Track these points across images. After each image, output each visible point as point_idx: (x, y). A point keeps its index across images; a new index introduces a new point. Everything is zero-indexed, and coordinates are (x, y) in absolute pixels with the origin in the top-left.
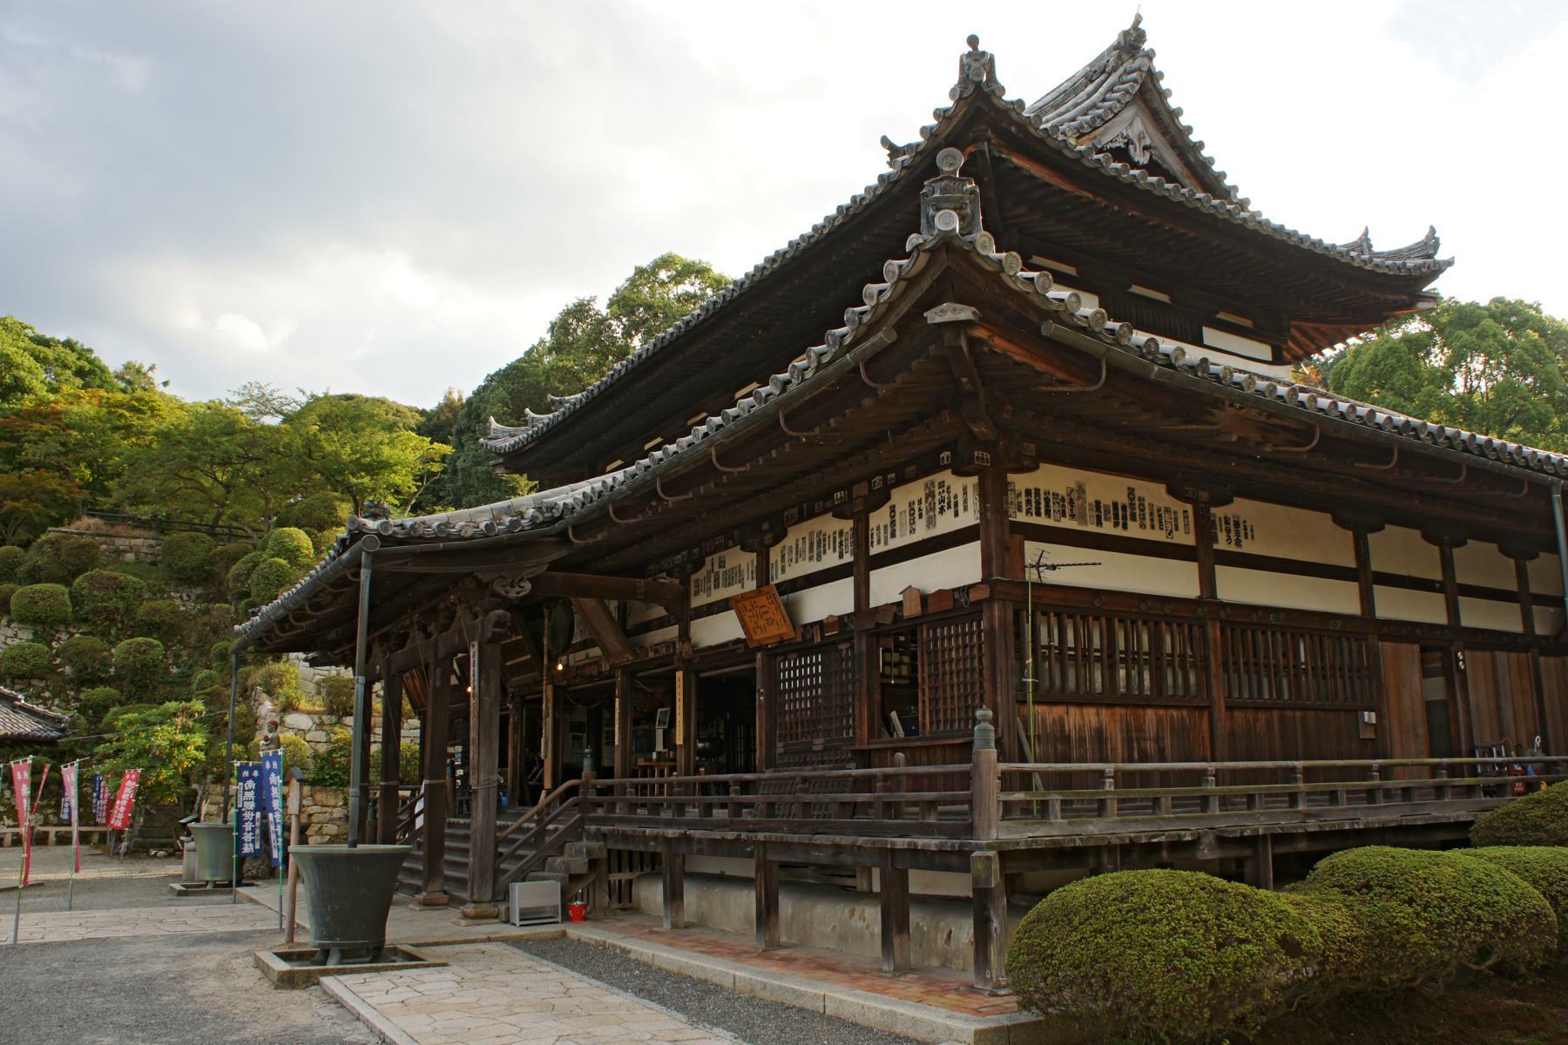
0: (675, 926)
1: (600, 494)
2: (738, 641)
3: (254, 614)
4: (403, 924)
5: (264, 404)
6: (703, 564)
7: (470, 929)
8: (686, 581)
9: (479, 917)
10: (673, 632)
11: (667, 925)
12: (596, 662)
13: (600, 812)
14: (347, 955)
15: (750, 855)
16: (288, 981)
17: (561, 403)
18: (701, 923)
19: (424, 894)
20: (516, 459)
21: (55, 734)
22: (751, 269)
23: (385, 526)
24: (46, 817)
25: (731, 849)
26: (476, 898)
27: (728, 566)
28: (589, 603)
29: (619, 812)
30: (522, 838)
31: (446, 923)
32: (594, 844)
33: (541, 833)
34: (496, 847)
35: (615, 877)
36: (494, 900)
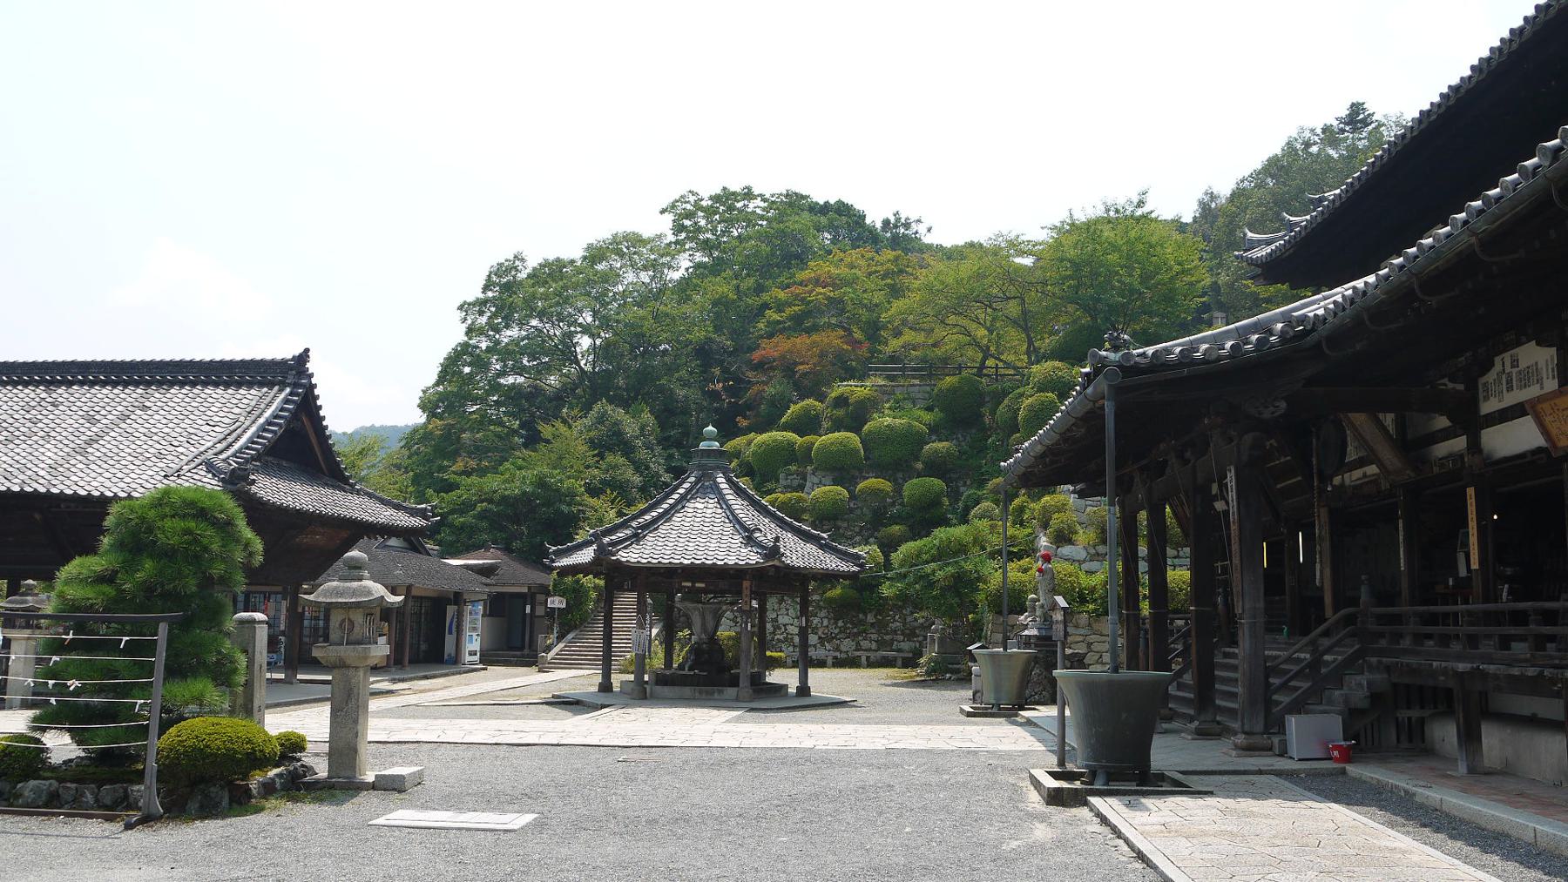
0: (1472, 771)
1: (1352, 301)
2: (1539, 450)
3: (1017, 451)
4: (1165, 753)
5: (1016, 246)
6: (1493, 365)
7: (1241, 760)
8: (1472, 385)
9: (1249, 749)
10: (1459, 443)
11: (1462, 769)
12: (1375, 481)
13: (1383, 643)
14: (1111, 777)
15: (1558, 695)
16: (1056, 798)
17: (1320, 200)
18: (1506, 771)
19: (1196, 723)
20: (1272, 270)
21: (856, 569)
22: (1531, 12)
23: (1128, 356)
24: (858, 644)
25: (1535, 686)
26: (1247, 728)
27: (1523, 365)
28: (1359, 418)
29: (1406, 643)
30: (1295, 668)
31: (1215, 754)
32: (1378, 677)
33: (1315, 664)
34: (1267, 677)
35: (1403, 714)
36: (1267, 731)
